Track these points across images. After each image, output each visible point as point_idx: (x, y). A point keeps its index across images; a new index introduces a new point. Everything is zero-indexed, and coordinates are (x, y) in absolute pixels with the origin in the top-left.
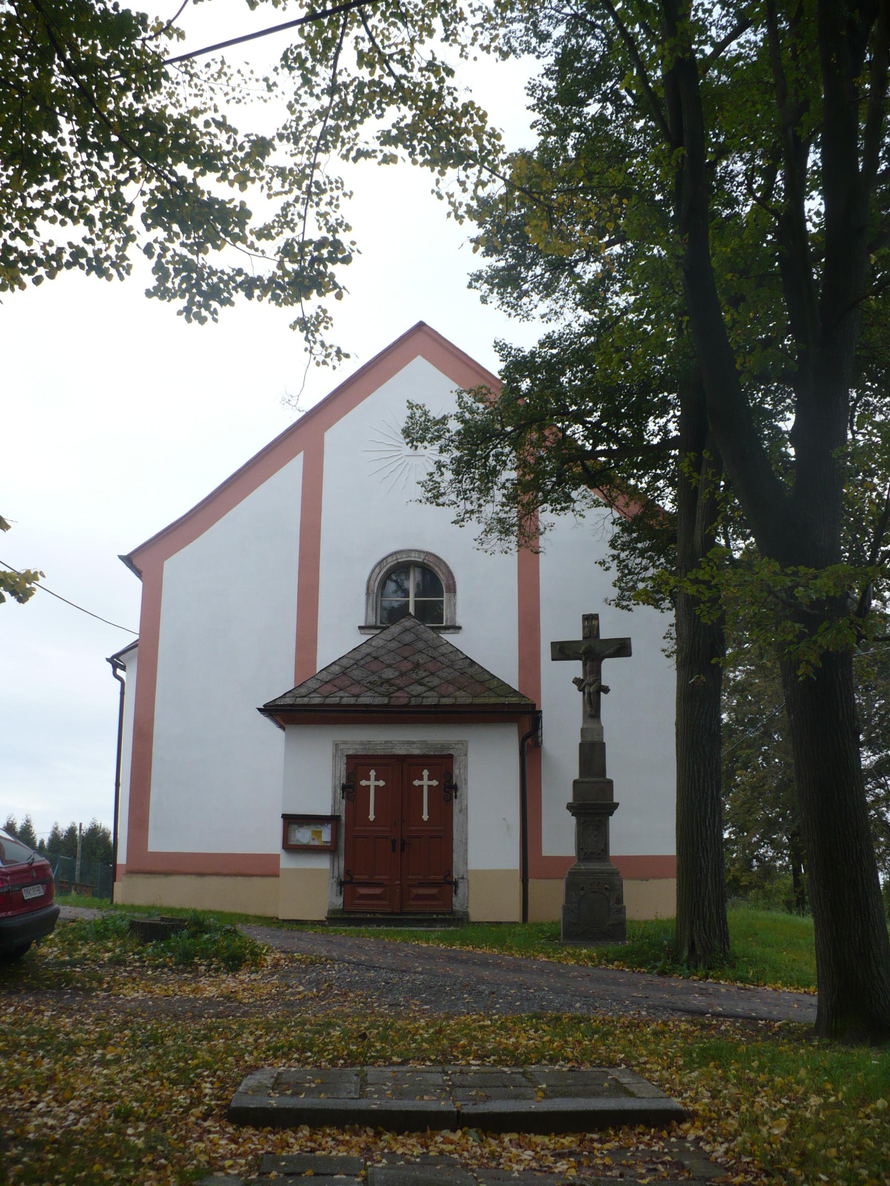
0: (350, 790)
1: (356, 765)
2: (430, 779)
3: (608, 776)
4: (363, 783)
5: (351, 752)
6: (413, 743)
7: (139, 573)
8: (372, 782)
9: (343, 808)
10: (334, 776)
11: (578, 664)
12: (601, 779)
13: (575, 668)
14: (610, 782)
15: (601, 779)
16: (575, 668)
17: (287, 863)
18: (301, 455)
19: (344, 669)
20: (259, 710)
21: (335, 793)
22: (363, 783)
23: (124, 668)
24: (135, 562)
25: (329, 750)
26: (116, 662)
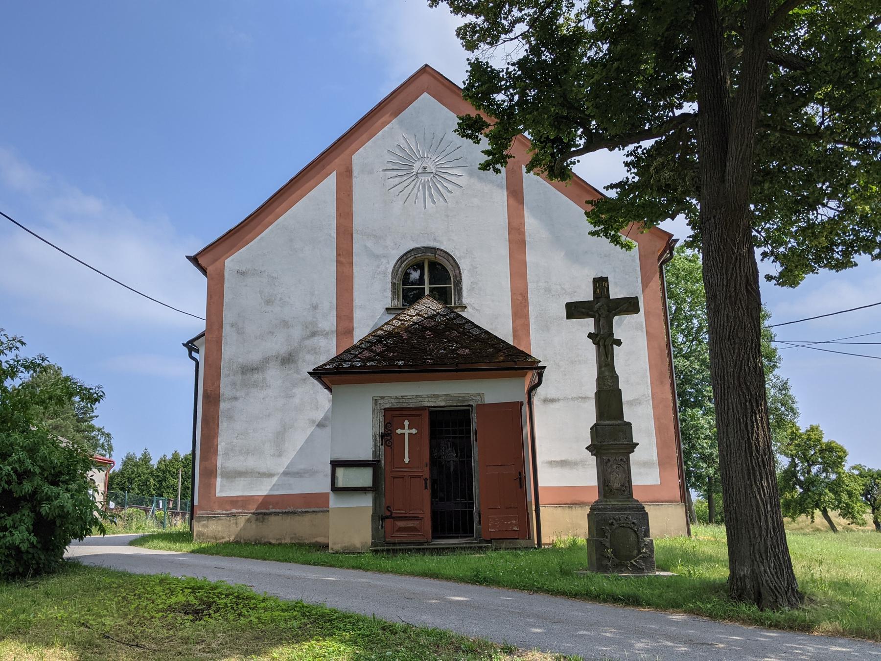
0: (387, 437)
1: (392, 416)
2: (410, 428)
3: (626, 419)
4: (399, 431)
5: (388, 406)
6: (437, 396)
7: (204, 271)
8: (406, 430)
9: (382, 452)
10: (374, 426)
11: (591, 321)
12: (619, 422)
13: (588, 325)
14: (629, 424)
15: (619, 422)
16: (588, 325)
17: (334, 502)
18: (335, 172)
19: (377, 339)
20: (309, 373)
21: (375, 440)
22: (399, 431)
23: (198, 351)
24: (201, 261)
25: (369, 406)
26: (191, 346)
